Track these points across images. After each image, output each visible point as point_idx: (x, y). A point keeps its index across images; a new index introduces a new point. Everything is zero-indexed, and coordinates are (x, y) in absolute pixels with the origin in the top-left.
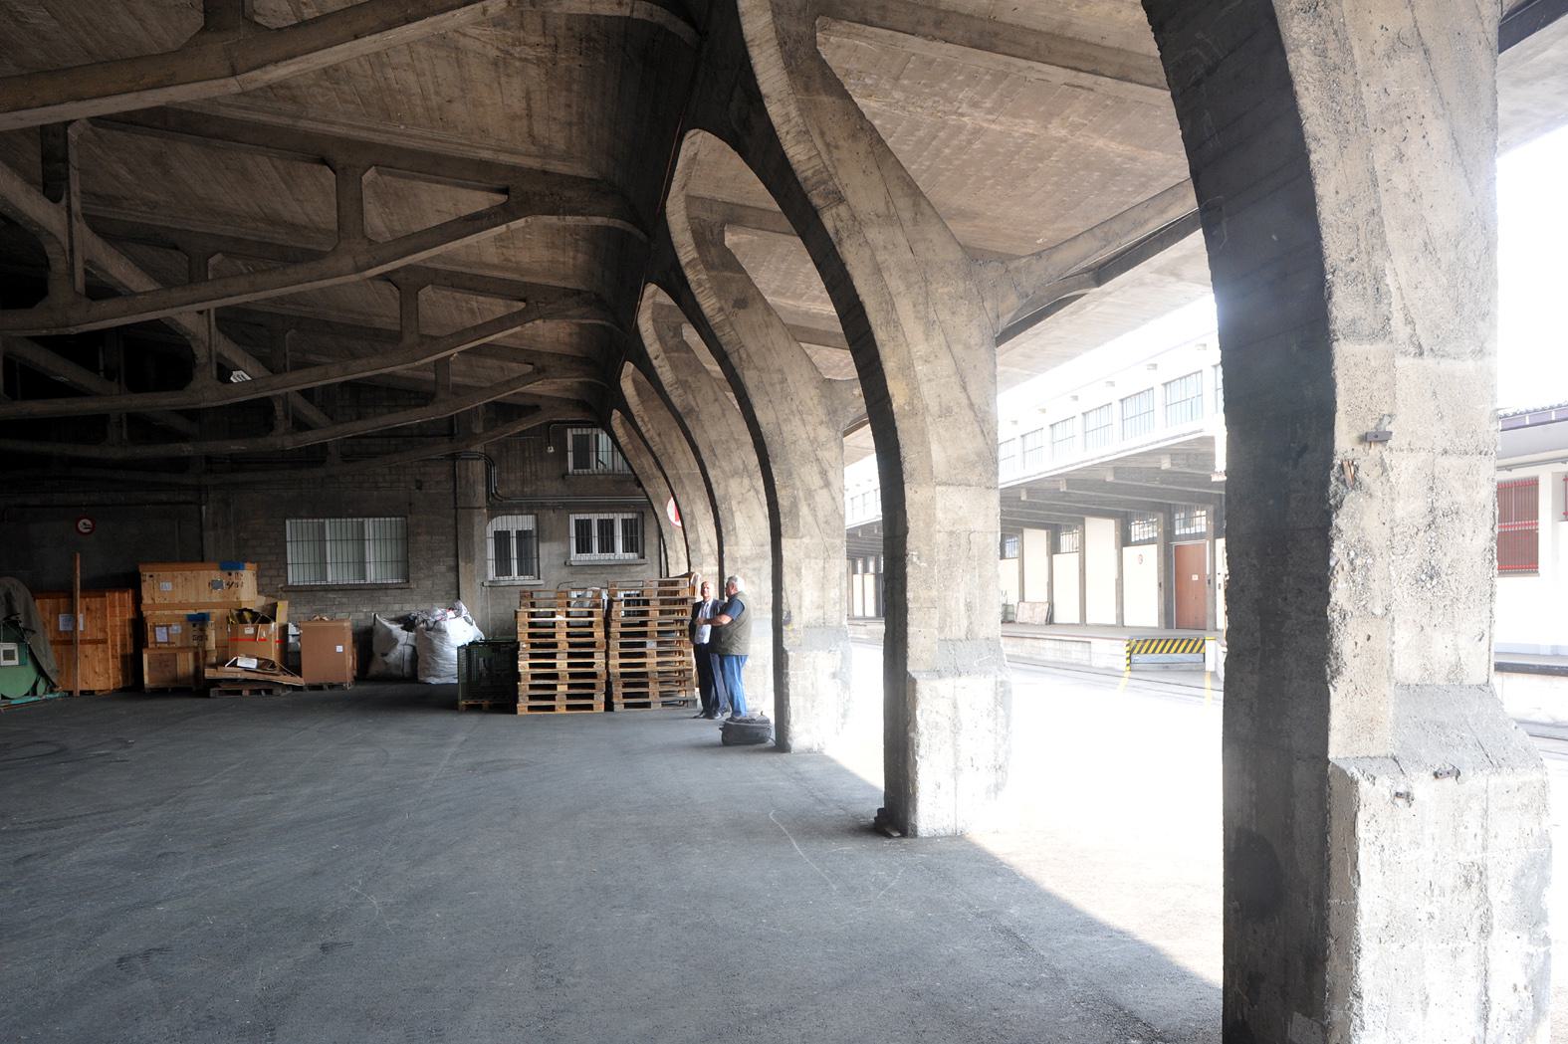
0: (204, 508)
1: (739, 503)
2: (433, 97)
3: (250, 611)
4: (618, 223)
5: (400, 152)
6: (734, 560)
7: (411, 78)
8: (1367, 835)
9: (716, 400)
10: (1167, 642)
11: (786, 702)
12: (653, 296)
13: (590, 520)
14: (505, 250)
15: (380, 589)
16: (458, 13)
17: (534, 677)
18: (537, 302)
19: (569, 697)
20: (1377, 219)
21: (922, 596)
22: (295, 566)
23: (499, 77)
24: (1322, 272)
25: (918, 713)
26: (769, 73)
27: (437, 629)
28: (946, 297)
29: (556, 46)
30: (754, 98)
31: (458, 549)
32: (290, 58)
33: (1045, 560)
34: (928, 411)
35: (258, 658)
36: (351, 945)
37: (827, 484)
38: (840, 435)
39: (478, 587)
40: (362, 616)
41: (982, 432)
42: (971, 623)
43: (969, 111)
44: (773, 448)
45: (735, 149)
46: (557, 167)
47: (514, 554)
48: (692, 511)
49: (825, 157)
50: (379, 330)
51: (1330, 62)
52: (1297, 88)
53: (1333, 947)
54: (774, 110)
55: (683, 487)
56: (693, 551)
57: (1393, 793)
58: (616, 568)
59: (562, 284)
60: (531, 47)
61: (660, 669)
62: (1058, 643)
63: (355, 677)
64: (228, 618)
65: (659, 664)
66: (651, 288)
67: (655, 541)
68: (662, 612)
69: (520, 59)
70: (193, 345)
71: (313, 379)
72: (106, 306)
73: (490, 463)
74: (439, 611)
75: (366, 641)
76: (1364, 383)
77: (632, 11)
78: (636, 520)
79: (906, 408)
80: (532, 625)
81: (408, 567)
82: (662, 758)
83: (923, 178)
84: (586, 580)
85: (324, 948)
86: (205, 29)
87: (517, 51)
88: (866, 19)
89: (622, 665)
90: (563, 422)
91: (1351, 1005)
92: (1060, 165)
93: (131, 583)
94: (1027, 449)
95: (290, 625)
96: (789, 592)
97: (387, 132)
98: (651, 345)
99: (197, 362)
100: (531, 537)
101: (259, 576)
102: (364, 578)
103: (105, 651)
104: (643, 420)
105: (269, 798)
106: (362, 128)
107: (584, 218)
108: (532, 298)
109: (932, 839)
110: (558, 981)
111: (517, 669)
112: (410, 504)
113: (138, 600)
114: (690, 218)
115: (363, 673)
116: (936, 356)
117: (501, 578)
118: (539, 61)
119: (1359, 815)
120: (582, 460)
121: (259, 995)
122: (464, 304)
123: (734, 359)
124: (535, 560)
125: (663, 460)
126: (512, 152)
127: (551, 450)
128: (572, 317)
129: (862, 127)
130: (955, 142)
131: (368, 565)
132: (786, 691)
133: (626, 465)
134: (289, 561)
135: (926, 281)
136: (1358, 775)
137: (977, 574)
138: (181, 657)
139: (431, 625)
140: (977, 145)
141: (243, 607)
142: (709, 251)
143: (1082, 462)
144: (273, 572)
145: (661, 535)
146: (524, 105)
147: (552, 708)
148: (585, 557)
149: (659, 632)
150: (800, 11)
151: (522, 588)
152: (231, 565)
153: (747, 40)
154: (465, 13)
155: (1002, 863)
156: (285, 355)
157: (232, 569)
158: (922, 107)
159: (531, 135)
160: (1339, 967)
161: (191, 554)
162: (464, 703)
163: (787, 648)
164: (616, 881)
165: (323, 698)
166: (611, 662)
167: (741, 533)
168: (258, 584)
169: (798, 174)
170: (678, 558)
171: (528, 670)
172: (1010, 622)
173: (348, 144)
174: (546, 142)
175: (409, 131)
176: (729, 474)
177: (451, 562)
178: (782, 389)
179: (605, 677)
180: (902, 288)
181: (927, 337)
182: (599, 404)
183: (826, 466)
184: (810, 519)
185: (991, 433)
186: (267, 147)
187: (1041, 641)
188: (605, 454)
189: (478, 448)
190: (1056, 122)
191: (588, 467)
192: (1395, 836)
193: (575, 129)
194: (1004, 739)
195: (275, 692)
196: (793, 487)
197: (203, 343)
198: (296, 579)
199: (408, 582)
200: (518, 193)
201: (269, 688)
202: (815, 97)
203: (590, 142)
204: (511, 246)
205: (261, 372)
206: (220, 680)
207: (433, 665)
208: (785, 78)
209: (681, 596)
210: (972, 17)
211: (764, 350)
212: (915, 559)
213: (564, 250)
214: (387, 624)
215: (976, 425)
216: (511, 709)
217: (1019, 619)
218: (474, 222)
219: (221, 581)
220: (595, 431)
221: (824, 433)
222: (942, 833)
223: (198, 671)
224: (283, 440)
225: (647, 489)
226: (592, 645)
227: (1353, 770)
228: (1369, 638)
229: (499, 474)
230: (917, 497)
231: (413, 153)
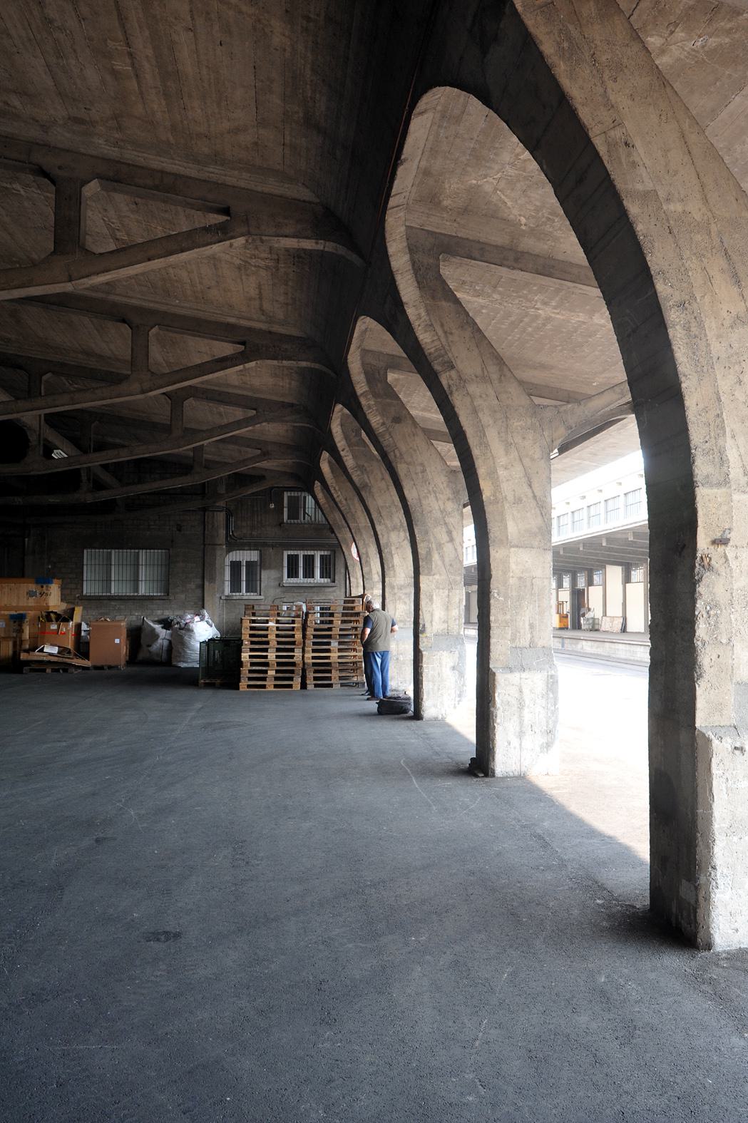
0: (26, 539)
1: (397, 548)
2: (198, 285)
3: (55, 613)
4: (317, 366)
6: (393, 588)
7: (184, 274)
8: (717, 772)
9: (383, 479)
11: (421, 686)
12: (339, 411)
13: (298, 555)
14: (243, 377)
15: (149, 599)
16: (214, 247)
17: (252, 664)
18: (264, 411)
20: (720, 419)
21: (500, 619)
22: (89, 582)
23: (241, 275)
24: (689, 448)
25: (496, 695)
26: (408, 289)
27: (187, 629)
28: (519, 428)
29: (278, 260)
30: (399, 304)
31: (205, 573)
32: (107, 272)
33: (621, 587)
34: (507, 500)
35: (59, 647)
36: (115, 839)
37: (452, 540)
38: (461, 507)
39: (217, 600)
40: (134, 618)
41: (542, 513)
42: (533, 637)
43: (542, 307)
44: (416, 516)
45: (388, 331)
46: (276, 328)
47: (244, 577)
48: (367, 553)
49: (443, 340)
51: (692, 334)
52: (674, 348)
53: (700, 839)
54: (411, 312)
55: (361, 535)
56: (367, 579)
57: (733, 747)
58: (316, 588)
59: (281, 400)
60: (262, 260)
61: (340, 661)
62: (628, 646)
63: (127, 662)
64: (39, 617)
65: (339, 657)
66: (339, 407)
67: (343, 570)
68: (343, 622)
69: (255, 266)
70: (28, 433)
71: (110, 457)
73: (229, 514)
74: (189, 616)
75: (137, 636)
76: (714, 510)
77: (324, 247)
78: (330, 555)
79: (492, 498)
80: (252, 628)
81: (169, 584)
82: (341, 724)
83: (515, 345)
85: (97, 841)
86: (54, 253)
87: (253, 261)
88: (471, 256)
89: (313, 658)
90: (281, 487)
91: (710, 873)
92: (602, 340)
94: (561, 524)
95: (83, 623)
96: (424, 612)
97: (167, 304)
98: (339, 442)
99: (30, 444)
100: (257, 566)
101: (62, 588)
102: (137, 592)
104: (335, 489)
105: (64, 744)
106: (152, 301)
107: (294, 362)
108: (258, 407)
109: (504, 778)
110: (247, 863)
111: (241, 658)
112: (172, 541)
114: (363, 364)
115: (133, 659)
116: (512, 465)
117: (234, 594)
118: (267, 268)
119: (713, 760)
120: (294, 514)
121: (54, 869)
122: (215, 409)
123: (391, 456)
124: (258, 582)
125: (348, 517)
126: (250, 319)
127: (272, 506)
128: (287, 422)
129: (467, 322)
130: (535, 325)
131: (140, 567)
132: (420, 678)
133: (324, 518)
134: (85, 578)
135: (507, 417)
136: (712, 737)
137: (537, 605)
140: (549, 327)
141: (50, 610)
142: (377, 385)
143: (636, 523)
144: (73, 586)
145: (347, 568)
146: (257, 292)
147: (264, 686)
149: (339, 635)
150: (429, 250)
151: (247, 603)
152: (44, 580)
153: (394, 270)
154: (219, 246)
155: (546, 794)
156: (90, 438)
157: (44, 583)
158: (512, 304)
159: (261, 309)
160: (703, 851)
162: (202, 681)
163: (422, 649)
164: (293, 802)
165: (104, 677)
166: (306, 655)
167: (398, 569)
168: (62, 594)
169: (425, 350)
170: (358, 583)
171: (248, 659)
172: (597, 630)
173: (141, 311)
174: (271, 314)
175: (182, 305)
176: (390, 529)
177: (199, 581)
178: (423, 477)
179: (301, 665)
180: (491, 422)
181: (507, 452)
182: (307, 477)
183: (451, 528)
184: (439, 563)
185: (547, 515)
186: (88, 311)
187: (616, 644)
189: (222, 504)
190: (597, 315)
191: (298, 519)
192: (734, 772)
193: (290, 307)
194: (553, 713)
195: (70, 670)
196: (429, 541)
197: (35, 431)
198: (89, 591)
199: (168, 595)
200: (252, 345)
201: (66, 667)
202: (439, 303)
204: (247, 374)
205: (75, 452)
207: (183, 654)
208: (417, 292)
209: (357, 610)
210: (538, 256)
211: (411, 450)
212: (496, 595)
213: (283, 379)
214: (152, 624)
215: (537, 509)
217: (603, 628)
218: (223, 363)
219: (36, 592)
220: (303, 494)
221: (450, 506)
222: (511, 774)
223: (16, 655)
224: (86, 496)
225: (338, 535)
226: (293, 643)
227: (710, 733)
228: (719, 656)
230: (497, 555)
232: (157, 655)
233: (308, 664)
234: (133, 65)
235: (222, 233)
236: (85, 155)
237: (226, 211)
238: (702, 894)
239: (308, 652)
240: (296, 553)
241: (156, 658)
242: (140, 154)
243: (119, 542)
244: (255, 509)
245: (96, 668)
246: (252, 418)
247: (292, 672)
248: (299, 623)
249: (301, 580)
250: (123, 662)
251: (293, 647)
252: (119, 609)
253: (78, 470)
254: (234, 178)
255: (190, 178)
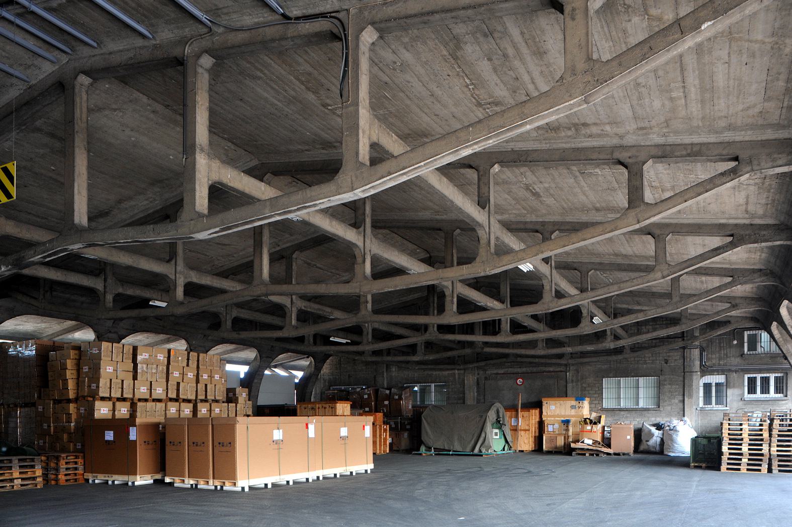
3: (589, 419)
5: (682, 225)
19: (748, 465)
31: (684, 390)
39: (694, 410)
40: (636, 423)
50: (654, 292)
59: (752, 267)
72: (563, 301)
73: (702, 350)
75: (638, 434)
78: (783, 377)
84: (752, 408)
89: (778, 451)
93: (539, 405)
100: (723, 386)
101: (590, 403)
102: (638, 405)
103: (529, 434)
113: (541, 413)
115: (636, 450)
117: (706, 406)
124: (725, 398)
138: (559, 438)
139: (672, 428)
144: (597, 402)
146: (745, 200)
147: (739, 470)
148: (752, 396)
152: (580, 399)
161: (563, 394)
165: (619, 458)
166: (772, 449)
171: (727, 450)
175: (688, 217)
177: (681, 398)
179: (768, 456)
188: (766, 343)
189: (697, 343)
201: (597, 453)
203: (777, 210)
205: (606, 318)
206: (576, 449)
213: (755, 253)
216: (718, 468)
218: (717, 251)
220: (760, 332)
226: (762, 440)
229: (707, 355)
231: (689, 225)
232: (654, 447)
233: (774, 455)
234: (684, 92)
235: (733, 173)
236: (644, 146)
237: (736, 159)
239: (774, 447)
240: (754, 375)
241: (653, 450)
242: (678, 137)
243: (626, 374)
244: (722, 345)
245: (615, 454)
246: (729, 283)
247: (761, 460)
248: (766, 426)
249: (758, 395)
250: (632, 452)
252: (627, 417)
253: (606, 330)
254: (739, 137)
255: (711, 143)
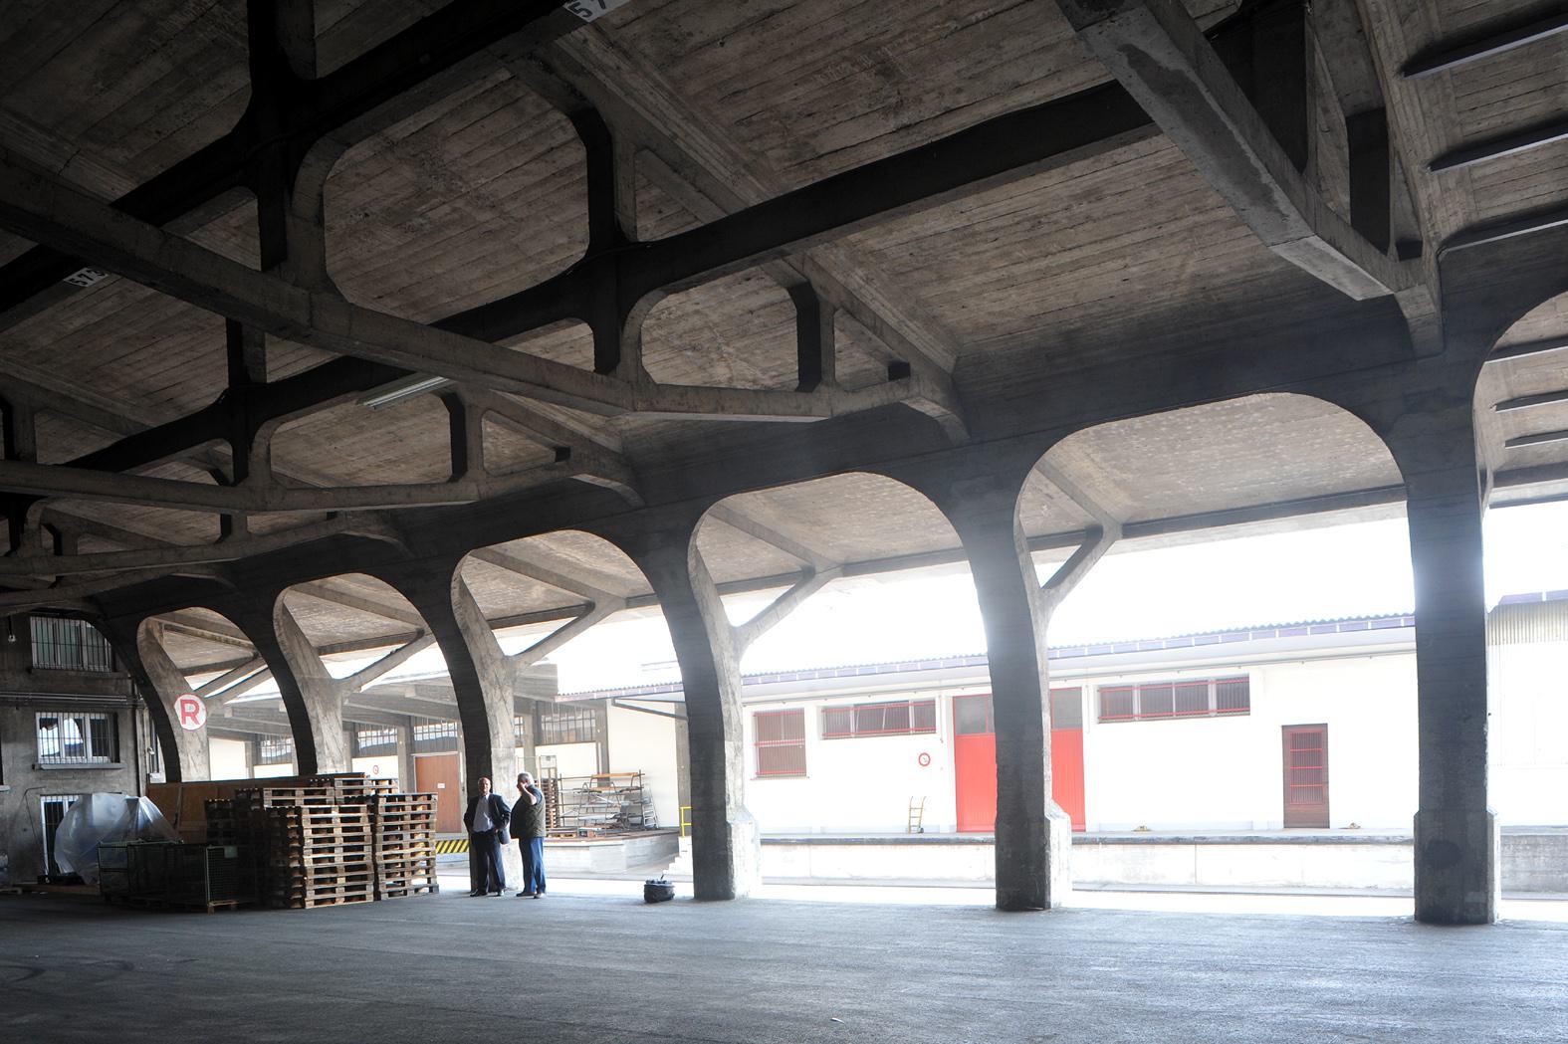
10: (456, 844)
226: (361, 838)
238: (1490, 895)
251: (361, 843)
